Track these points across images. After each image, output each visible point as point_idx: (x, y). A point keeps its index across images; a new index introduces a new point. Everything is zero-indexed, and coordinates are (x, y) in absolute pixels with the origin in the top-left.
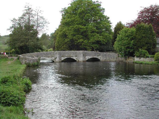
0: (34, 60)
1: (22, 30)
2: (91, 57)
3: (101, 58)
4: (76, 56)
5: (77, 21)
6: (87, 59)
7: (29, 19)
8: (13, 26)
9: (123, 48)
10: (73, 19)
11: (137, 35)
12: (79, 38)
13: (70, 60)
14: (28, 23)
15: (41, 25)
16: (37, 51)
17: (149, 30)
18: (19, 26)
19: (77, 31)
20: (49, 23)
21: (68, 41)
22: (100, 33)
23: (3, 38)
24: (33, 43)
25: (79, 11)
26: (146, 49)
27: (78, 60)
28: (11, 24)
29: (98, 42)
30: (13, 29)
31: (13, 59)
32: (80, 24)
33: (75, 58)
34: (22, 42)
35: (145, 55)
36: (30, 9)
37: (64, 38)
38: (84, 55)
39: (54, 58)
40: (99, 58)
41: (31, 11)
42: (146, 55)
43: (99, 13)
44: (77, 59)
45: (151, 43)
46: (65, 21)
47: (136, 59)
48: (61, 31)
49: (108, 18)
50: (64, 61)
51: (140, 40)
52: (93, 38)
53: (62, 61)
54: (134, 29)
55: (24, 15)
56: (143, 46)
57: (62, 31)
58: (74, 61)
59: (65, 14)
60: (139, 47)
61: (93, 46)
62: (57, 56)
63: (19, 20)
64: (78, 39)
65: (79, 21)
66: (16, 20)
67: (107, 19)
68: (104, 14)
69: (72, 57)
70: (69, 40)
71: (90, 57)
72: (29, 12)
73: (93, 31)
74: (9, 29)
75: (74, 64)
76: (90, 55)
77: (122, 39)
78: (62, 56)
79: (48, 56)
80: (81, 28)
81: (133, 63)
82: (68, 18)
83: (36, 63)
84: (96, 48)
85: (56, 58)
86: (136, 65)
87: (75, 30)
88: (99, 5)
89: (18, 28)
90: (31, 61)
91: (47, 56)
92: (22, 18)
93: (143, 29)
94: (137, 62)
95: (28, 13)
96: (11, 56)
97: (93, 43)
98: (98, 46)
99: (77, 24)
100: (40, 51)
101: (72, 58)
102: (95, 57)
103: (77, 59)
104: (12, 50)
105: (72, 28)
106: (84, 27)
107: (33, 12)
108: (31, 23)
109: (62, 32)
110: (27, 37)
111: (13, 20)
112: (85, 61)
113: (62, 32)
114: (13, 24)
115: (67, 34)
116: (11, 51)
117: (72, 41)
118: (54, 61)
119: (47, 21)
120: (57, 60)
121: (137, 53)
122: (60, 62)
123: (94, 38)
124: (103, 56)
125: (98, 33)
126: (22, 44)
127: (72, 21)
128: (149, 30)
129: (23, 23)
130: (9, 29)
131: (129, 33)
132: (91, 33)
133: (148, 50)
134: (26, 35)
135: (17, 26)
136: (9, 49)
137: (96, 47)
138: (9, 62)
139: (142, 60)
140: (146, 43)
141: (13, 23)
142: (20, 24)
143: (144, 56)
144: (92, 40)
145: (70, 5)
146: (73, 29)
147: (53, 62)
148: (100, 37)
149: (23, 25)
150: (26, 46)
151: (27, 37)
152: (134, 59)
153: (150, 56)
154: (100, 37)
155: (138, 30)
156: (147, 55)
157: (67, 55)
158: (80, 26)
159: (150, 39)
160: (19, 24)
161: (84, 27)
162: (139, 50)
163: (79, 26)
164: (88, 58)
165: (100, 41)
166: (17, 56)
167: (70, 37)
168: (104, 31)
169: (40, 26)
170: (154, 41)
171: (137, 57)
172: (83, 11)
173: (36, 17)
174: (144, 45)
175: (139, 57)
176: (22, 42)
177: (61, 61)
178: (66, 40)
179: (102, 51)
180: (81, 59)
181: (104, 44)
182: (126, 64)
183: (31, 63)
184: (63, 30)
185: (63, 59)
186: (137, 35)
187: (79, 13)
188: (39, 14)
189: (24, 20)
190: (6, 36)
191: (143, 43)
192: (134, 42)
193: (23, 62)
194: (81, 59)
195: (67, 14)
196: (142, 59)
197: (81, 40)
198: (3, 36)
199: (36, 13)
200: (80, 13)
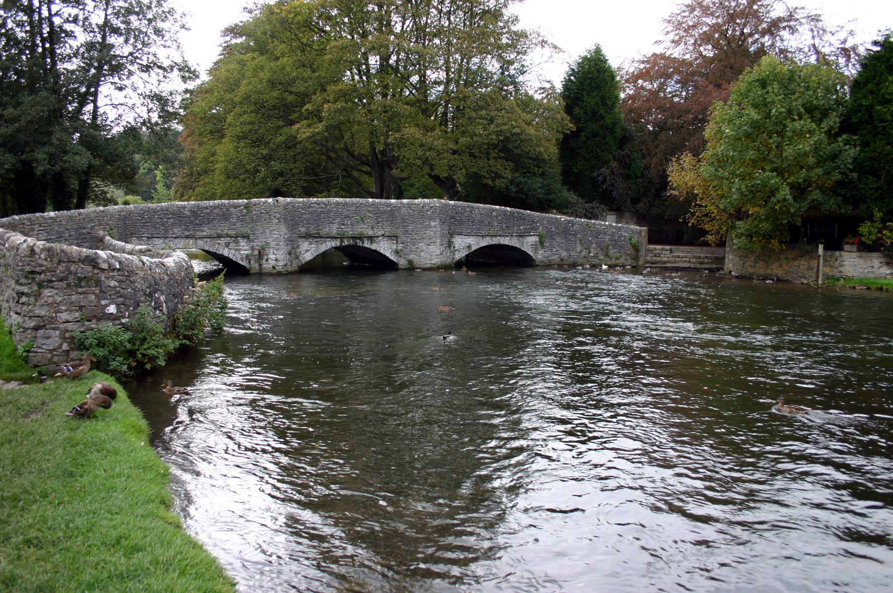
2: (485, 242)
33: (385, 248)
40: (528, 244)
58: (382, 265)
71: (476, 243)
78: (307, 236)
101: (367, 244)
103: (397, 252)
157: (334, 229)
185: (308, 252)
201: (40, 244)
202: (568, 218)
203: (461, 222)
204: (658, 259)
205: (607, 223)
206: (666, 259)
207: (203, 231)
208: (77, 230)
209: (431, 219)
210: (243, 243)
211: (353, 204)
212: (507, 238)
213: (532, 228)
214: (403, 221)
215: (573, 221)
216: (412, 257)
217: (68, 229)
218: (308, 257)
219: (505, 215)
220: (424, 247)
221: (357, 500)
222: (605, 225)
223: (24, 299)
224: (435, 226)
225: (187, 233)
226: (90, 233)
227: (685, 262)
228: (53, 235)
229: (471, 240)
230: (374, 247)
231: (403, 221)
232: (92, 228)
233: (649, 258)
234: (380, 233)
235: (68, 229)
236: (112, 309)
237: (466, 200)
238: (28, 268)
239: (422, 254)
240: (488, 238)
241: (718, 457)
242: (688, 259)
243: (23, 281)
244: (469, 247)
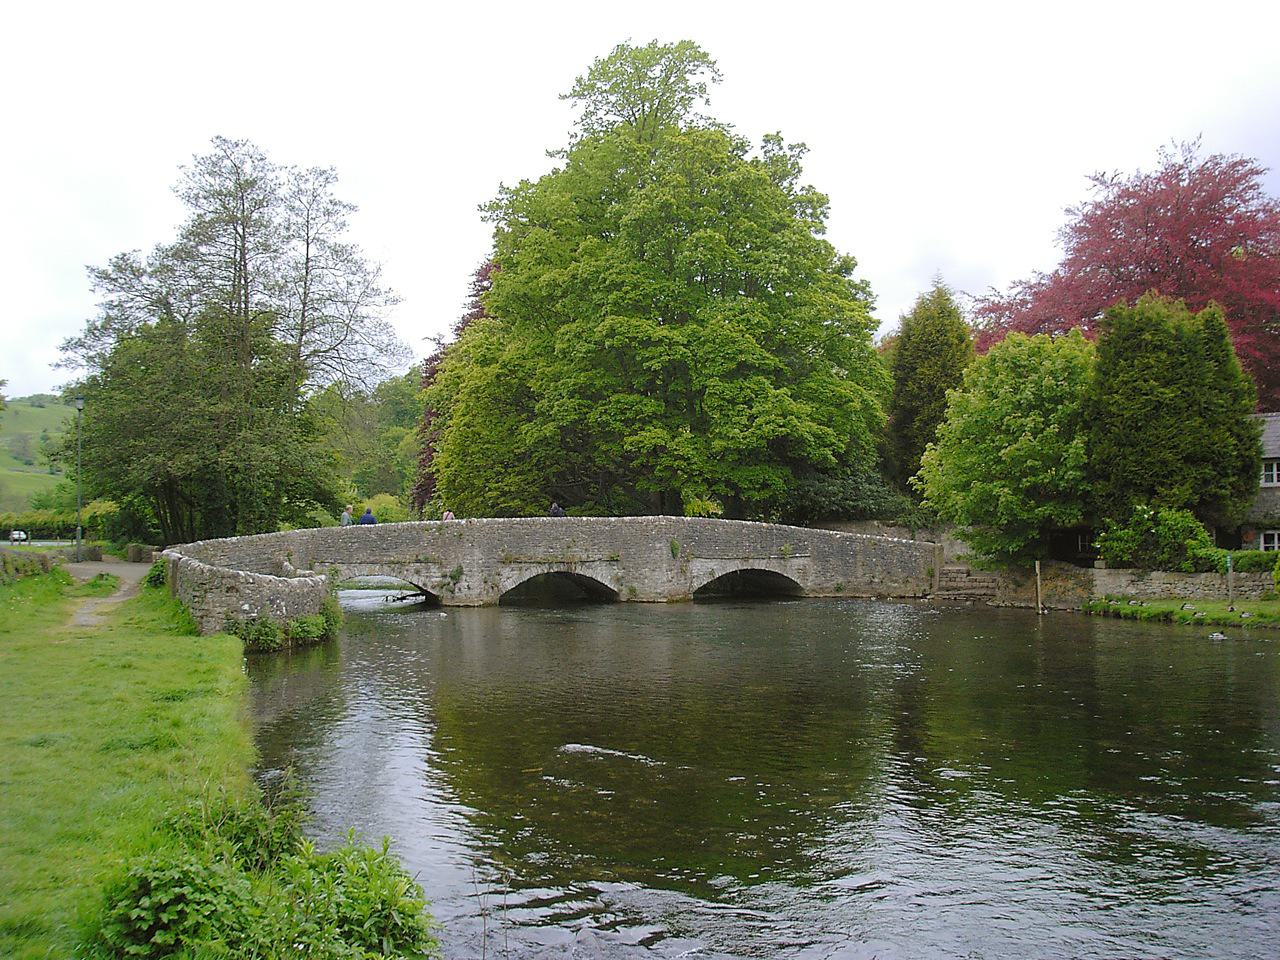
0: (297, 600)
1: (180, 354)
2: (733, 566)
3: (803, 572)
4: (613, 560)
5: (617, 286)
6: (696, 585)
7: (239, 265)
8: (109, 319)
9: (1004, 493)
10: (584, 268)
11: (1111, 391)
12: (633, 421)
14: (234, 295)
15: (330, 310)
16: (297, 518)
17: (1201, 350)
18: (154, 321)
19: (619, 360)
20: (395, 301)
21: (544, 441)
22: (792, 376)
23: (17, 413)
24: (270, 451)
25: (636, 208)
26: (1187, 505)
27: (632, 591)
28: (88, 305)
29: (783, 450)
30: (110, 342)
31: (100, 586)
32: (640, 309)
33: (603, 575)
34: (185, 442)
35: (1181, 549)
36: (252, 184)
37: (510, 421)
39: (444, 576)
40: (794, 569)
41: (259, 204)
42: (1190, 553)
43: (785, 226)
44: (618, 580)
45: (1222, 455)
46: (512, 282)
47: (1107, 584)
48: (485, 362)
49: (847, 266)
50: (522, 598)
51: (1139, 429)
52: (744, 421)
54: (1078, 347)
55: (201, 232)
56: (1167, 477)
57: (495, 360)
58: (595, 595)
59: (522, 229)
60: (1128, 484)
61: (743, 476)
62: (473, 559)
63: (163, 271)
64: (627, 422)
65: (635, 287)
66: (138, 273)
67: (839, 271)
68: (822, 231)
69: (583, 562)
70: (549, 429)
71: (721, 568)
73: (742, 365)
74: (80, 344)
75: (601, 626)
77: (982, 431)
78: (505, 562)
79: (394, 556)
80: (647, 343)
81: (1088, 613)
82: (545, 260)
83: (315, 625)
84: (766, 494)
85: (456, 577)
86: (1103, 633)
87: (598, 359)
88: (783, 167)
89: (147, 334)
90: (279, 608)
91: (381, 551)
92: (181, 254)
93: (1160, 348)
94: (1126, 608)
95: (233, 220)
96: (94, 556)
97: (748, 457)
98: (777, 478)
99: (618, 309)
100: (321, 514)
101: (580, 570)
102: (760, 565)
103: (618, 580)
104: (84, 505)
105: (578, 336)
106: (676, 335)
107: (278, 215)
108: (256, 298)
109: (494, 369)
110: (223, 407)
111: (110, 270)
112: (685, 601)
113: (494, 369)
114: (110, 306)
115: (533, 385)
116: (85, 514)
117: (576, 437)
118: (443, 594)
119: (381, 283)
121: (1120, 537)
122: (487, 605)
123: (752, 418)
124: (821, 557)
125: (778, 377)
126: (179, 464)
127: (581, 288)
128: (1201, 350)
129: (189, 294)
130: (80, 344)
131: (1048, 381)
132: (728, 376)
133: (1205, 508)
134: (214, 391)
135: (141, 314)
136: (66, 497)
137: (765, 486)
138: (88, 613)
139: (1156, 592)
140: (1189, 459)
141: (114, 297)
142: (167, 305)
143: (1175, 558)
144: (735, 433)
145: (561, 164)
146: (583, 347)
147: (431, 603)
148: (794, 406)
149: (190, 310)
150: (207, 476)
151: (223, 407)
152: (1088, 585)
153: (1226, 556)
154: (794, 406)
155: (1119, 354)
156: (1202, 552)
157: (540, 553)
159: (1213, 425)
160: (162, 304)
161: (676, 335)
162: (1131, 512)
163: (633, 322)
164: (705, 570)
165: (801, 441)
166: (139, 558)
167: (560, 407)
169: (325, 320)
170: (1248, 438)
171: (1117, 564)
172: (665, 206)
173: (297, 250)
174: (1171, 473)
175: (1139, 561)
176: (185, 442)
177: (493, 597)
178: (530, 433)
179: (804, 513)
181: (822, 469)
182: (1021, 620)
183: (277, 618)
184: (506, 357)
185: (510, 580)
186: (1111, 391)
187: (639, 223)
188: (321, 228)
189: (204, 270)
190: (38, 402)
191: (1168, 455)
192: (1089, 453)
193: (206, 614)
195: (535, 233)
196: (1158, 580)
197: (654, 435)
198: (13, 401)
199: (294, 219)
200: (643, 228)
201: (208, 567)
202: (846, 534)
203: (699, 544)
204: (954, 584)
205: (896, 539)
206: (962, 585)
207: (390, 556)
208: (256, 555)
209: (656, 539)
210: (434, 569)
211: (562, 524)
212: (762, 561)
213: (799, 549)
214: (625, 542)
215: (851, 537)
216: (635, 585)
217: (249, 555)
218: (510, 585)
219: (760, 532)
220: (648, 574)
221: (609, 867)
222: (892, 542)
223: (196, 599)
224: (660, 548)
225: (372, 559)
226: (269, 559)
227: (982, 587)
228: (234, 560)
229: (713, 564)
230: (589, 573)
231: (625, 542)
232: (272, 553)
233: (944, 583)
234: (597, 557)
235: (249, 555)
236: (246, 607)
237: (619, 516)
238: (199, 582)
239: (646, 581)
240: (737, 561)
241: (426, 723)
242: (986, 584)
243: (197, 588)
244: (712, 573)
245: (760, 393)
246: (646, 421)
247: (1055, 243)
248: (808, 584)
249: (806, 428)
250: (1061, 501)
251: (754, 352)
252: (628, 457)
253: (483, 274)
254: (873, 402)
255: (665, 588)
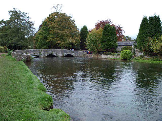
2: (67, 54)
13: (52, 56)
33: (55, 55)
38: (63, 52)
40: (73, 54)
47: (104, 56)
49: (33, 24)
50: (48, 56)
53: (46, 57)
58: (54, 56)
72: (85, 25)
75: (55, 59)
76: (67, 52)
78: (46, 53)
101: (53, 54)
102: (70, 54)
117: (51, 42)
120: (42, 56)
124: (75, 53)
158: (59, 31)
164: (65, 54)
168: (124, 37)
180: (60, 55)
181: (75, 46)
185: (46, 55)
194: (60, 55)
196: (108, 56)
245: (70, 38)
246: (59, 41)
247: (62, 5)
248: (74, 56)
249: (74, 42)
250: (137, 44)
251: (68, 34)
252: (57, 44)
253: (41, 26)
254: (78, 39)
255: (61, 56)
